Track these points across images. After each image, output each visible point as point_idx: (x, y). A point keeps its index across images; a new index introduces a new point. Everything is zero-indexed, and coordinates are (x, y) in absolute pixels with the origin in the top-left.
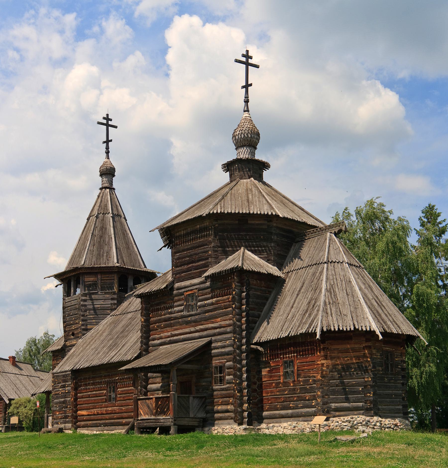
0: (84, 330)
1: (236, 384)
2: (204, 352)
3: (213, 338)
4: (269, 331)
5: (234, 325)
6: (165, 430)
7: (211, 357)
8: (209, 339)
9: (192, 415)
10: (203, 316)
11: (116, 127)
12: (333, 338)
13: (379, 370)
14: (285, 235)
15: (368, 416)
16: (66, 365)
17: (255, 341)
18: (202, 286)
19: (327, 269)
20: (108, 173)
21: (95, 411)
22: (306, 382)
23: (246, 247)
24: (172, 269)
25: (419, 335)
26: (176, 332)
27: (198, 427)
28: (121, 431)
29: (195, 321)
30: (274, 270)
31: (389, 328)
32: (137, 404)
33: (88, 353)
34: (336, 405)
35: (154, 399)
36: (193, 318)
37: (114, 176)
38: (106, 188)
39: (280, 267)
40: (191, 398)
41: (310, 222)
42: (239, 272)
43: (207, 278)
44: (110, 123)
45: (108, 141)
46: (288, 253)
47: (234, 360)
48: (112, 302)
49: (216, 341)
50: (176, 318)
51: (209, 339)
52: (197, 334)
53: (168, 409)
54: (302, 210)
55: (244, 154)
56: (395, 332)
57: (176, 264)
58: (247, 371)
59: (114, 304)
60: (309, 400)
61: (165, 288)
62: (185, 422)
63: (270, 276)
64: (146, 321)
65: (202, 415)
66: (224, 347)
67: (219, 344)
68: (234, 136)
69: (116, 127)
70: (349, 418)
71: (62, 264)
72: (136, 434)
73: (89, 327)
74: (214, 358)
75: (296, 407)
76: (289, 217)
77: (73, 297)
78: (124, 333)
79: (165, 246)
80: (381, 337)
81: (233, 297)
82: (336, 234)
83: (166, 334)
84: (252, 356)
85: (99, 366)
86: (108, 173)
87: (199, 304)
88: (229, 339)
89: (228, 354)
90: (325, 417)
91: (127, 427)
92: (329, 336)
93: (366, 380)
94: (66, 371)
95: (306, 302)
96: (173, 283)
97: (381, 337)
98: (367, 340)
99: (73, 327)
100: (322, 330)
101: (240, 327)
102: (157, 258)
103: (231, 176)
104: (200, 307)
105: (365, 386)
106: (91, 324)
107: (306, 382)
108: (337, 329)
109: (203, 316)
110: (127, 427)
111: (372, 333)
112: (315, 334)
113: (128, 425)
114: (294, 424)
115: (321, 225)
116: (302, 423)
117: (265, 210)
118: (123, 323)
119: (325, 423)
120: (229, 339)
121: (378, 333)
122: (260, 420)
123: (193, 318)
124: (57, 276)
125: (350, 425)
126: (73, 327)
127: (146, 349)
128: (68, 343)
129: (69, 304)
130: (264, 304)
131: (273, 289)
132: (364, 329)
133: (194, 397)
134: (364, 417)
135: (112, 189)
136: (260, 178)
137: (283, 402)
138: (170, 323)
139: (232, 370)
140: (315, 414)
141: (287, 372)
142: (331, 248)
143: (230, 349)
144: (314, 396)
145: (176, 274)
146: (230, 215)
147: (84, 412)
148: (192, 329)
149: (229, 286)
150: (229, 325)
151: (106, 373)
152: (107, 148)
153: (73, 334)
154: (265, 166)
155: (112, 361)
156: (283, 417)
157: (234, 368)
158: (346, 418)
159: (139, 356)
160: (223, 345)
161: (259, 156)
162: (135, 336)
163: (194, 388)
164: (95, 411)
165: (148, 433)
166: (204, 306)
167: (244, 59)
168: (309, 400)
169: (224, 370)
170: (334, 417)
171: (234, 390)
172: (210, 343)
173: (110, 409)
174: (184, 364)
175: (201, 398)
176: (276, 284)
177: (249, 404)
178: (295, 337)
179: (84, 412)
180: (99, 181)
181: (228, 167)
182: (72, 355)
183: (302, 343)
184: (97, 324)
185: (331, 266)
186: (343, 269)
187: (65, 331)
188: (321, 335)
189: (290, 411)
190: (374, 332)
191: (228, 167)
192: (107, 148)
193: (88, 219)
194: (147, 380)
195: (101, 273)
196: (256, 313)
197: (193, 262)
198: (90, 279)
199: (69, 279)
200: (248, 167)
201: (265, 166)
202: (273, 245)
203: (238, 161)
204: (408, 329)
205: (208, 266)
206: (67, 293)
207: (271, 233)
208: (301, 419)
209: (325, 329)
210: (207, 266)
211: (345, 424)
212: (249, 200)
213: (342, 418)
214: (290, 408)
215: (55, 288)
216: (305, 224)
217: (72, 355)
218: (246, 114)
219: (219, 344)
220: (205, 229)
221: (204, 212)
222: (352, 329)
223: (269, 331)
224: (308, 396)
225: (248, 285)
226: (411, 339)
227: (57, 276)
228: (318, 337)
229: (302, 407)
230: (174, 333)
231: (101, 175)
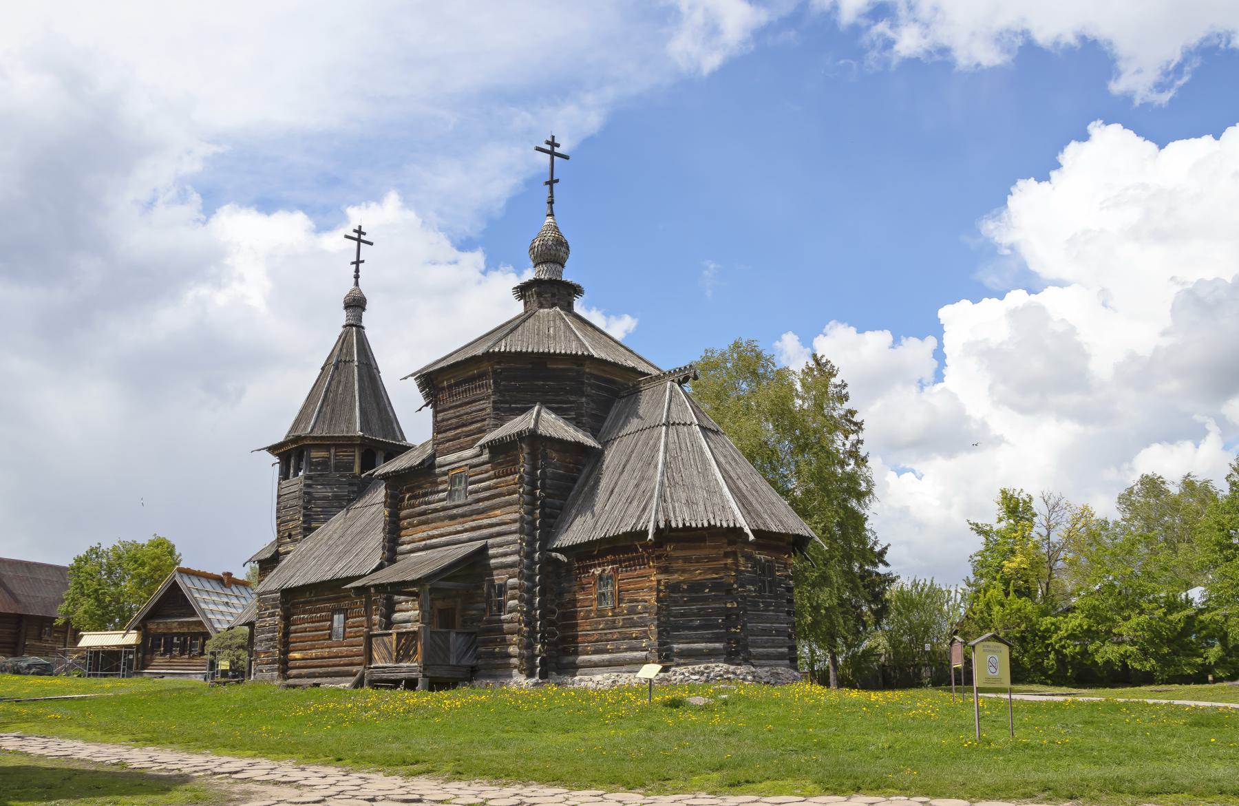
0: (305, 529)
1: (521, 612)
2: (477, 563)
3: (490, 541)
4: (578, 531)
5: (522, 519)
6: (411, 684)
7: (489, 571)
8: (483, 542)
9: (453, 661)
10: (475, 507)
11: (371, 244)
12: (674, 539)
13: (750, 591)
14: (602, 390)
15: (732, 664)
16: (275, 582)
17: (557, 544)
18: (475, 461)
19: (667, 434)
20: (356, 304)
21: (313, 653)
22: (632, 611)
23: (547, 404)
24: (433, 439)
25: (813, 534)
26: (436, 532)
27: (463, 680)
28: (346, 684)
29: (463, 515)
30: (590, 442)
31: (764, 524)
32: (370, 644)
33: (310, 564)
34: (681, 646)
35: (394, 636)
36: (460, 510)
37: (364, 309)
38: (352, 325)
39: (595, 434)
40: (453, 635)
41: (642, 367)
42: (533, 438)
43: (482, 447)
44: (363, 237)
45: (358, 262)
46: (608, 413)
47: (520, 575)
48: (352, 488)
49: (493, 546)
50: (436, 510)
51: (483, 542)
52: (465, 536)
53: (415, 652)
54: (631, 351)
55: (544, 273)
56: (774, 529)
57: (438, 428)
58: (542, 593)
59: (353, 492)
60: (636, 638)
61: (420, 464)
62: (442, 673)
63: (579, 445)
64: (391, 515)
65: (467, 661)
66: (505, 555)
67: (501, 550)
68: (532, 249)
69: (371, 244)
70: (702, 667)
71: (279, 435)
72: (367, 689)
73: (314, 525)
74: (495, 572)
75: (618, 650)
76: (609, 359)
77: (293, 480)
78: (364, 533)
79: (427, 405)
80: (752, 537)
81: (521, 477)
82: (680, 384)
83: (420, 535)
84: (550, 569)
85: (304, 586)
86: (356, 304)
87: (470, 487)
88: (514, 542)
89: (512, 565)
90: (659, 667)
91: (353, 679)
92: (667, 535)
93: (729, 605)
94: (271, 592)
95: (633, 483)
96: (433, 456)
97: (752, 537)
98: (731, 543)
99: (291, 525)
100: (657, 527)
101: (532, 523)
102: (416, 422)
103: (525, 304)
104: (471, 493)
105: (728, 617)
106: (317, 520)
107: (632, 611)
108: (681, 526)
109: (475, 507)
110: (353, 679)
111: (737, 532)
112: (646, 532)
113: (355, 675)
114: (613, 676)
115: (655, 373)
116: (626, 675)
117: (574, 349)
118: (363, 520)
119: (662, 675)
120: (514, 542)
121: (747, 530)
122: (573, 669)
123: (460, 510)
124: (272, 449)
125: (703, 678)
126: (291, 525)
127: (391, 555)
128: (282, 550)
129: (285, 491)
130: (570, 489)
131: (584, 465)
132: (725, 525)
133: (457, 633)
134: (726, 666)
135: (360, 328)
136: (568, 308)
137: (597, 641)
138: (425, 519)
139: (517, 591)
140: (645, 661)
141: (603, 594)
142: (673, 406)
143: (515, 558)
144: (645, 632)
145: (438, 444)
146: (519, 354)
147: (297, 655)
148: (459, 528)
149: (515, 462)
150: (515, 521)
151: (330, 593)
152: (357, 271)
153: (290, 536)
154: (576, 290)
155: (338, 576)
156: (596, 665)
157: (519, 587)
158: (696, 667)
159: (380, 567)
160: (506, 553)
161: (568, 275)
162: (377, 537)
163: (458, 619)
164: (313, 653)
165: (391, 688)
166: (476, 492)
167: (548, 147)
168: (636, 638)
169: (506, 592)
170: (678, 665)
171: (519, 622)
172: (485, 548)
173: (335, 650)
174: (443, 580)
175: (470, 634)
176: (593, 458)
177: (543, 644)
178: (616, 538)
179: (297, 655)
180: (342, 317)
181: (523, 291)
182: (285, 567)
183: (624, 548)
184: (326, 520)
185: (672, 430)
186: (691, 434)
187: (279, 532)
188: (655, 535)
189: (606, 657)
190: (741, 529)
191: (523, 291)
192: (357, 271)
193: (323, 369)
194: (391, 608)
195: (337, 446)
196: (557, 502)
197: (464, 425)
198: (317, 455)
199: (290, 454)
200: (549, 292)
201: (576, 290)
202: (584, 399)
203: (535, 283)
204: (797, 526)
205: (484, 431)
206: (284, 475)
207: (583, 383)
208: (624, 669)
209: (662, 525)
210: (482, 431)
211: (694, 677)
212: (552, 336)
213: (690, 667)
214: (607, 651)
215: (270, 466)
216: (633, 370)
217: (285, 567)
218: (549, 219)
219: (501, 550)
220: (481, 376)
221: (479, 351)
222: (706, 525)
223: (578, 531)
224: (635, 631)
225: (545, 457)
226: (798, 543)
227: (272, 449)
228: (650, 537)
229: (626, 650)
230: (430, 533)
231: (346, 308)
